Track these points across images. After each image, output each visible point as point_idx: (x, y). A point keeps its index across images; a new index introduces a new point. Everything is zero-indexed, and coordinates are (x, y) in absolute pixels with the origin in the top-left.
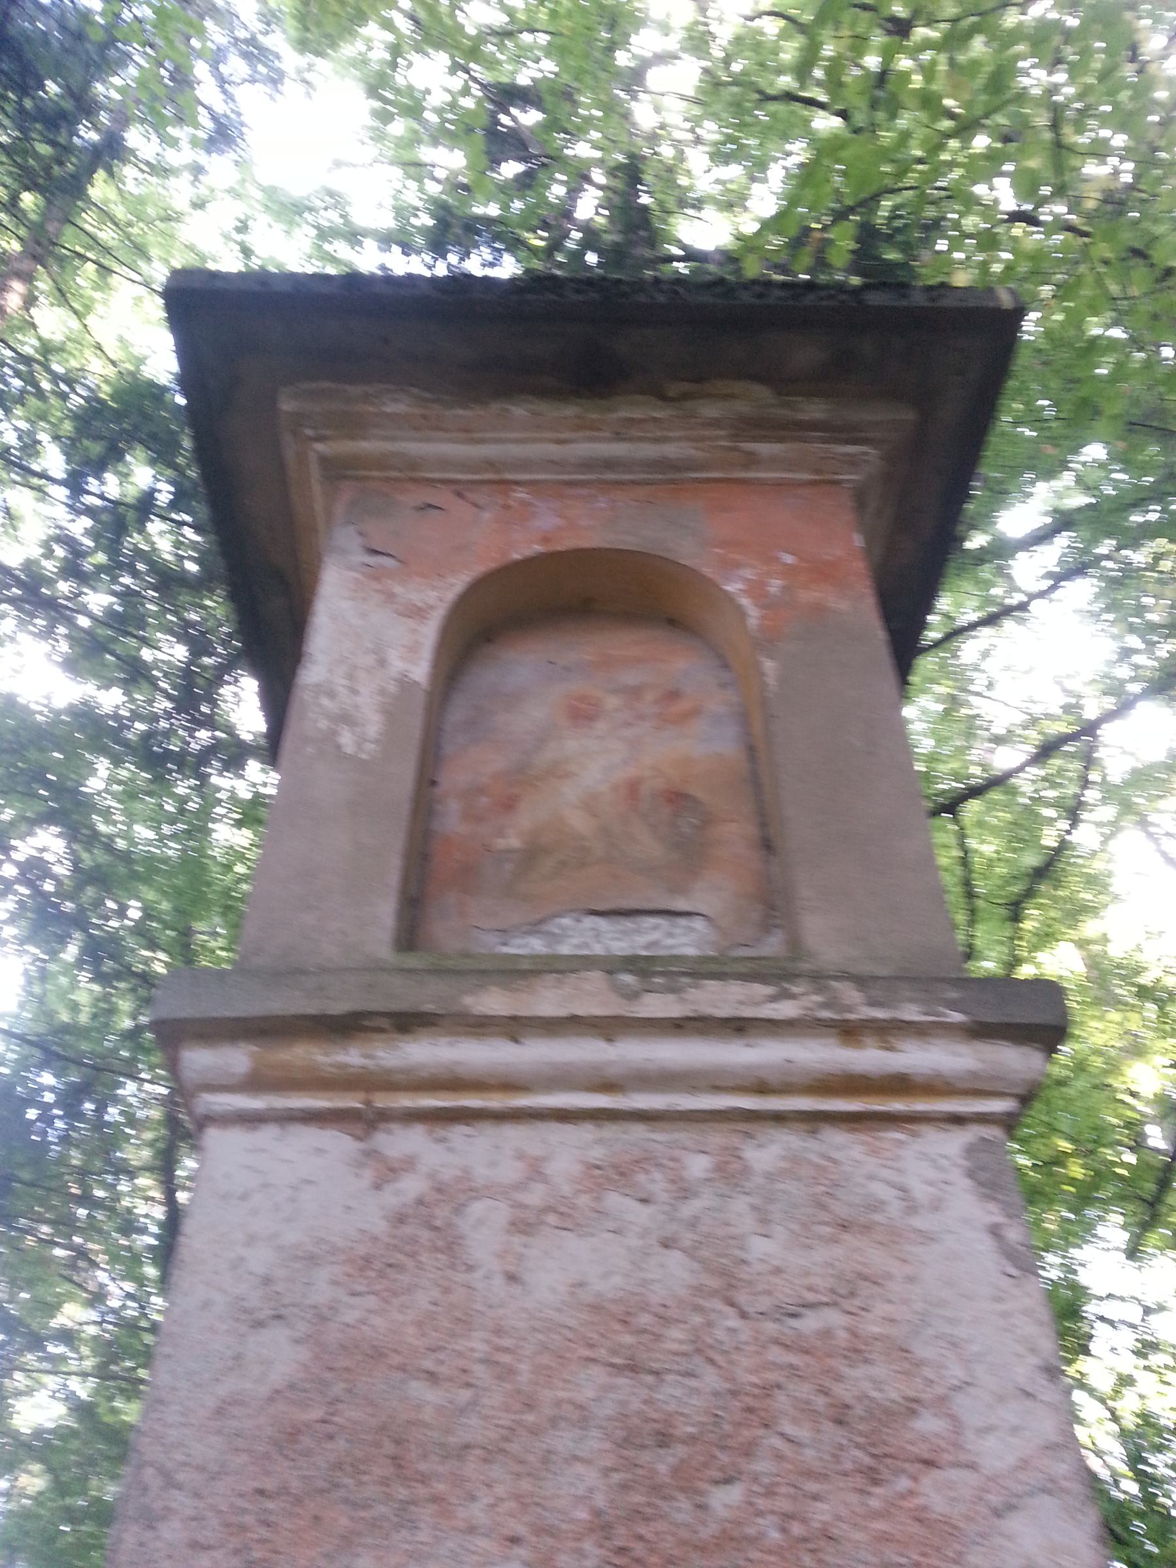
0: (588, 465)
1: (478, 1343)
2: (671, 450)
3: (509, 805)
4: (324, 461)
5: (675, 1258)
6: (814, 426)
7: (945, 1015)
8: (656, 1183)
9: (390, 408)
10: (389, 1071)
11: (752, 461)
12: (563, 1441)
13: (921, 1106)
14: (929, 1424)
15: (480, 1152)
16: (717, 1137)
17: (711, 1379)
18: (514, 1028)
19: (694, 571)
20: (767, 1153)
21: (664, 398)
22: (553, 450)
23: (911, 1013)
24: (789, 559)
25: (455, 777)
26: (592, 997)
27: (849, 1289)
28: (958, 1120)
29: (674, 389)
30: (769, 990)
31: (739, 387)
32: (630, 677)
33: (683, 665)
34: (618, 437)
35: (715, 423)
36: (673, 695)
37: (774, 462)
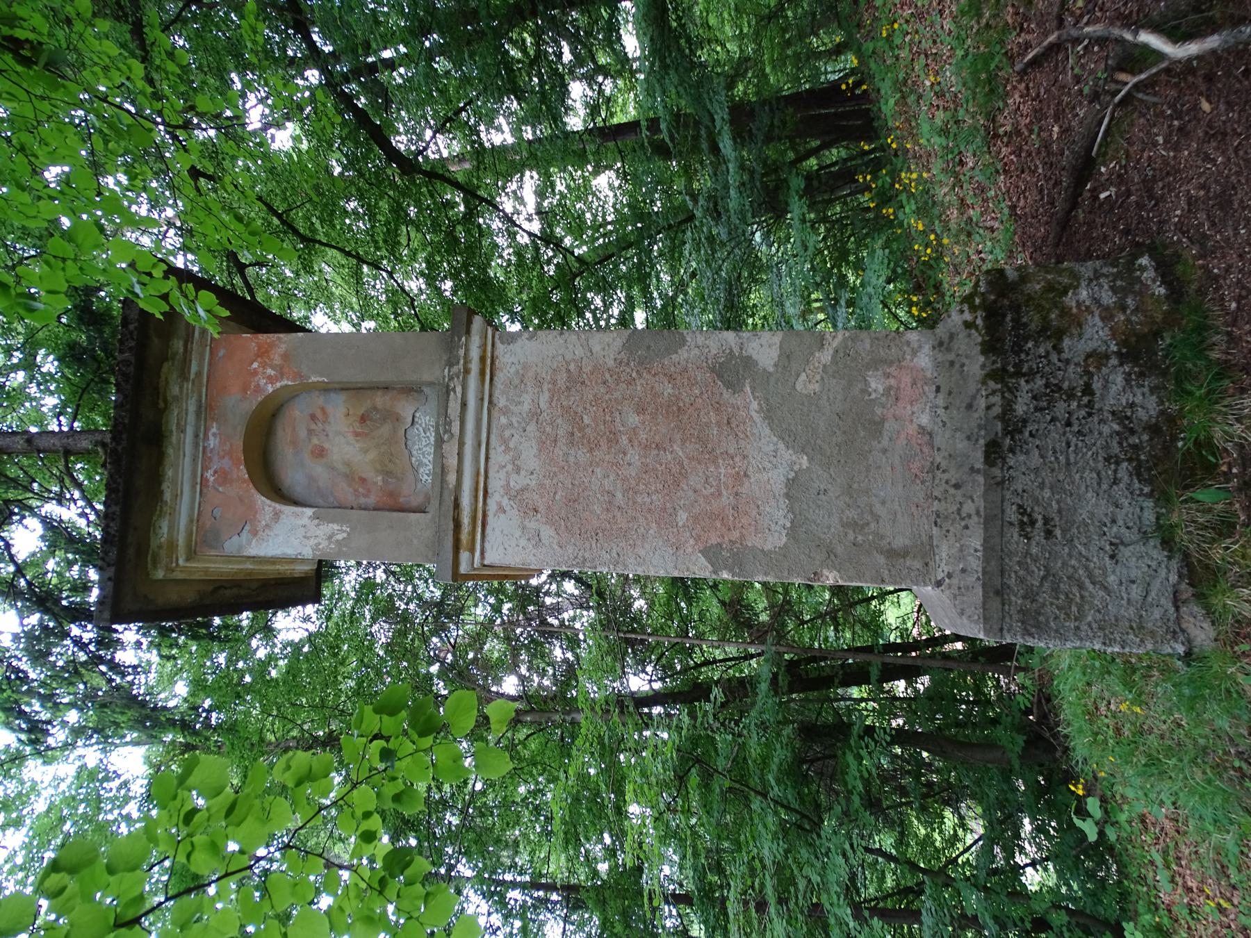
0: (196, 445)
1: (547, 482)
2: (192, 408)
3: (363, 480)
4: (188, 560)
5: (528, 428)
6: (186, 346)
9: (165, 530)
11: (199, 374)
12: (572, 459)
14: (572, 367)
15: (496, 484)
16: (495, 413)
17: (559, 421)
18: (460, 472)
19: (261, 403)
20: (501, 402)
21: (166, 408)
22: (187, 460)
23: (462, 352)
24: (255, 365)
25: (350, 499)
26: (451, 449)
27: (539, 382)
28: (493, 345)
29: (162, 405)
31: (163, 376)
32: (303, 434)
33: (297, 413)
34: (183, 431)
35: (181, 388)
36: (313, 417)
37: (200, 365)
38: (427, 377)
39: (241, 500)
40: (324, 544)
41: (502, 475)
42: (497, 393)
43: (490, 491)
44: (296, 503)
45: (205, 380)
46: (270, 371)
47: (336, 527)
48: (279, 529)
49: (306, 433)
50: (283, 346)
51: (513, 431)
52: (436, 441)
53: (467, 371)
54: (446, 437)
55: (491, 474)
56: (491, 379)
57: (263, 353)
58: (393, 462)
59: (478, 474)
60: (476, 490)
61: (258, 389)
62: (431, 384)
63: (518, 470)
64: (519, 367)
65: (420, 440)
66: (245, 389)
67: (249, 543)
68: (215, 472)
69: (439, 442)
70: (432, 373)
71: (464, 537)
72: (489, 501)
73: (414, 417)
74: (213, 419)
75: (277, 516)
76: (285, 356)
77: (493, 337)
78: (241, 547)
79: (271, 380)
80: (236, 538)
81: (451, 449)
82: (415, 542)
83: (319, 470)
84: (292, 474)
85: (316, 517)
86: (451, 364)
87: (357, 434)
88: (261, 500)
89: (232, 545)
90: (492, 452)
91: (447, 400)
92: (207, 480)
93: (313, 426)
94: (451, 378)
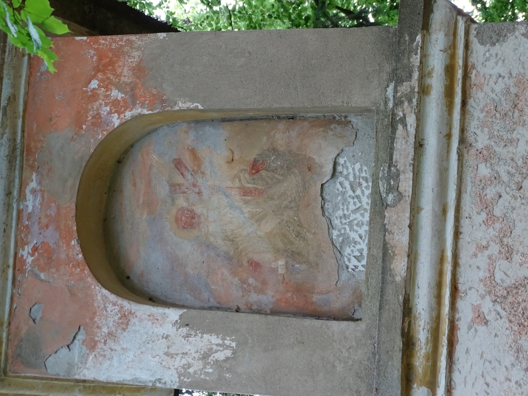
3: (255, 266)
7: (417, 45)
8: (490, 192)
10: (431, 318)
13: (460, 62)
15: (471, 276)
16: (470, 159)
20: (480, 139)
23: (416, 60)
24: (94, 84)
28: (467, 46)
30: (400, 127)
32: (162, 190)
33: (154, 159)
36: (178, 164)
37: (15, 86)
38: (358, 100)
39: (73, 294)
40: (197, 366)
41: (482, 261)
42: (473, 126)
43: (461, 287)
44: (152, 300)
45: (21, 108)
46: (116, 94)
47: (215, 340)
48: (128, 340)
49: (167, 188)
50: (136, 54)
51: (501, 189)
52: (374, 204)
53: (424, 90)
54: (390, 198)
55: (463, 259)
56: (464, 103)
57: (105, 65)
58: (302, 238)
59: (441, 260)
60: (439, 285)
61: (98, 122)
62: (363, 111)
63: (508, 254)
64: (511, 82)
65: (345, 201)
66: (79, 122)
67: (84, 360)
68: (35, 249)
69: (379, 206)
70: (368, 92)
71: (420, 362)
72: (460, 304)
73: (335, 164)
74: (32, 167)
75: (125, 319)
76: (139, 70)
77: (467, 33)
78: (71, 366)
79: (117, 107)
80: (64, 351)
81: (398, 218)
82: (339, 368)
83: (187, 248)
84: (147, 253)
85: (184, 323)
86: (398, 77)
87: (245, 192)
88: (101, 294)
89: (57, 363)
90: (465, 223)
91: (392, 139)
92: (23, 262)
93: (179, 179)
94: (398, 103)
